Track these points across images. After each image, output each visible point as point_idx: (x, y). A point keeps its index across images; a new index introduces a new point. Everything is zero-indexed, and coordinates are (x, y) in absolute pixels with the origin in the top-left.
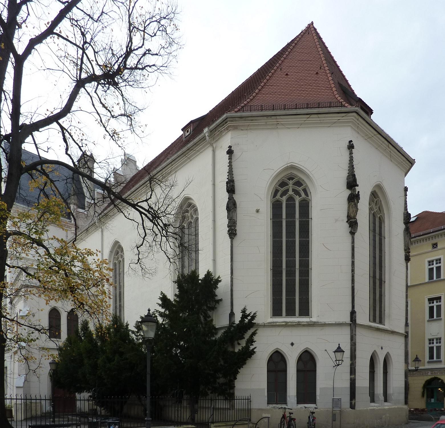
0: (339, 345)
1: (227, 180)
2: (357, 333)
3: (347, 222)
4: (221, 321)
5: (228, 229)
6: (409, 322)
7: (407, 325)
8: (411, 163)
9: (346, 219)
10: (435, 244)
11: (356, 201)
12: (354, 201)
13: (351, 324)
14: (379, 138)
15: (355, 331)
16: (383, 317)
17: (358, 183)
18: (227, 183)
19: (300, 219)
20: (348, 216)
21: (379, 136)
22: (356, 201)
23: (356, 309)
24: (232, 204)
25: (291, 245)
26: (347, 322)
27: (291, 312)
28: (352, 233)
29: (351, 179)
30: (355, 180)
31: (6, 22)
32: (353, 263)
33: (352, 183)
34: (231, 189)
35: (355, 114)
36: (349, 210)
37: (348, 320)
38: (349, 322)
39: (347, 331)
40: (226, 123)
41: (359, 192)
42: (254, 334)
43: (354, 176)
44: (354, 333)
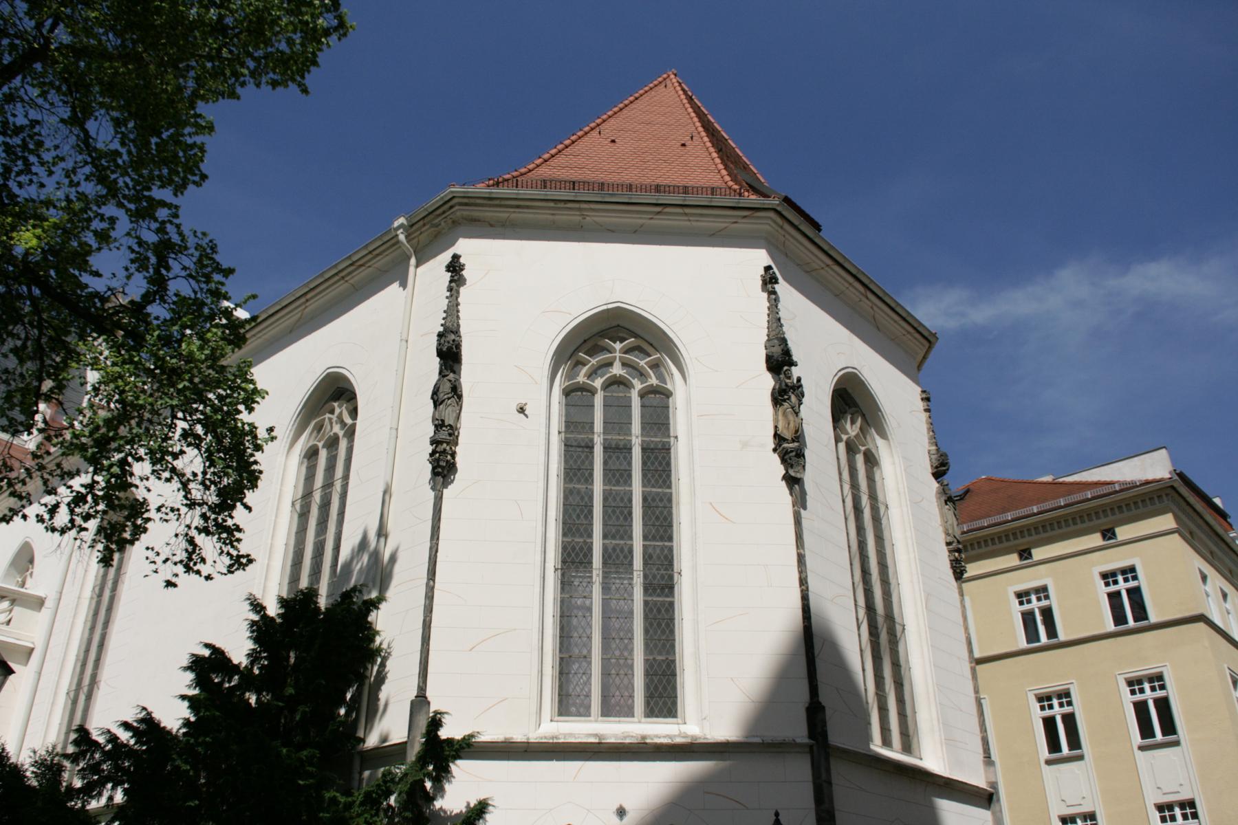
0: (777, 814)
1: (441, 329)
2: (835, 779)
3: (775, 450)
4: (392, 725)
5: (430, 449)
6: (995, 756)
7: (988, 759)
8: (929, 342)
9: (771, 444)
10: (1024, 551)
11: (793, 398)
12: (789, 398)
13: (811, 747)
14: (839, 275)
15: (828, 770)
16: (911, 732)
17: (795, 358)
18: (440, 335)
19: (665, 494)
20: (776, 435)
21: (837, 268)
22: (793, 398)
23: (823, 698)
24: (448, 385)
25: (618, 511)
26: (798, 740)
27: (614, 707)
28: (793, 482)
29: (777, 350)
30: (787, 353)
31: (5, 62)
32: (801, 559)
33: (779, 360)
34: (450, 356)
35: (772, 214)
36: (776, 420)
37: (798, 731)
38: (806, 740)
39: (800, 771)
40: (451, 207)
41: (799, 380)
42: (383, 665)
43: (784, 341)
44: (824, 776)
